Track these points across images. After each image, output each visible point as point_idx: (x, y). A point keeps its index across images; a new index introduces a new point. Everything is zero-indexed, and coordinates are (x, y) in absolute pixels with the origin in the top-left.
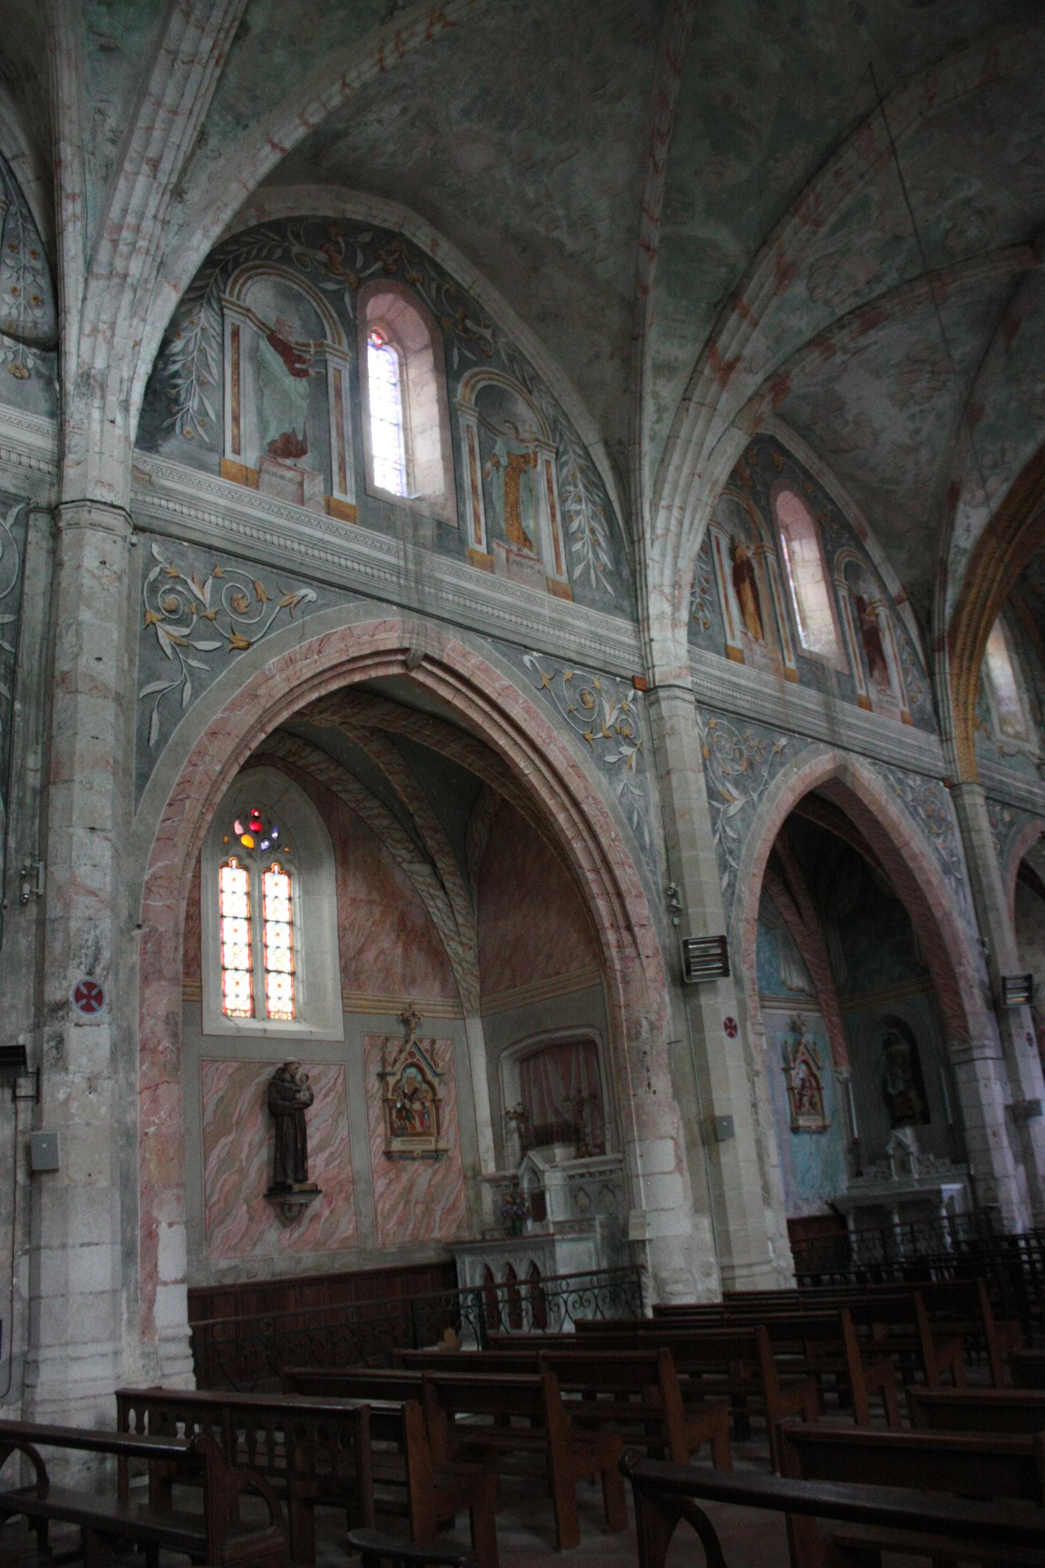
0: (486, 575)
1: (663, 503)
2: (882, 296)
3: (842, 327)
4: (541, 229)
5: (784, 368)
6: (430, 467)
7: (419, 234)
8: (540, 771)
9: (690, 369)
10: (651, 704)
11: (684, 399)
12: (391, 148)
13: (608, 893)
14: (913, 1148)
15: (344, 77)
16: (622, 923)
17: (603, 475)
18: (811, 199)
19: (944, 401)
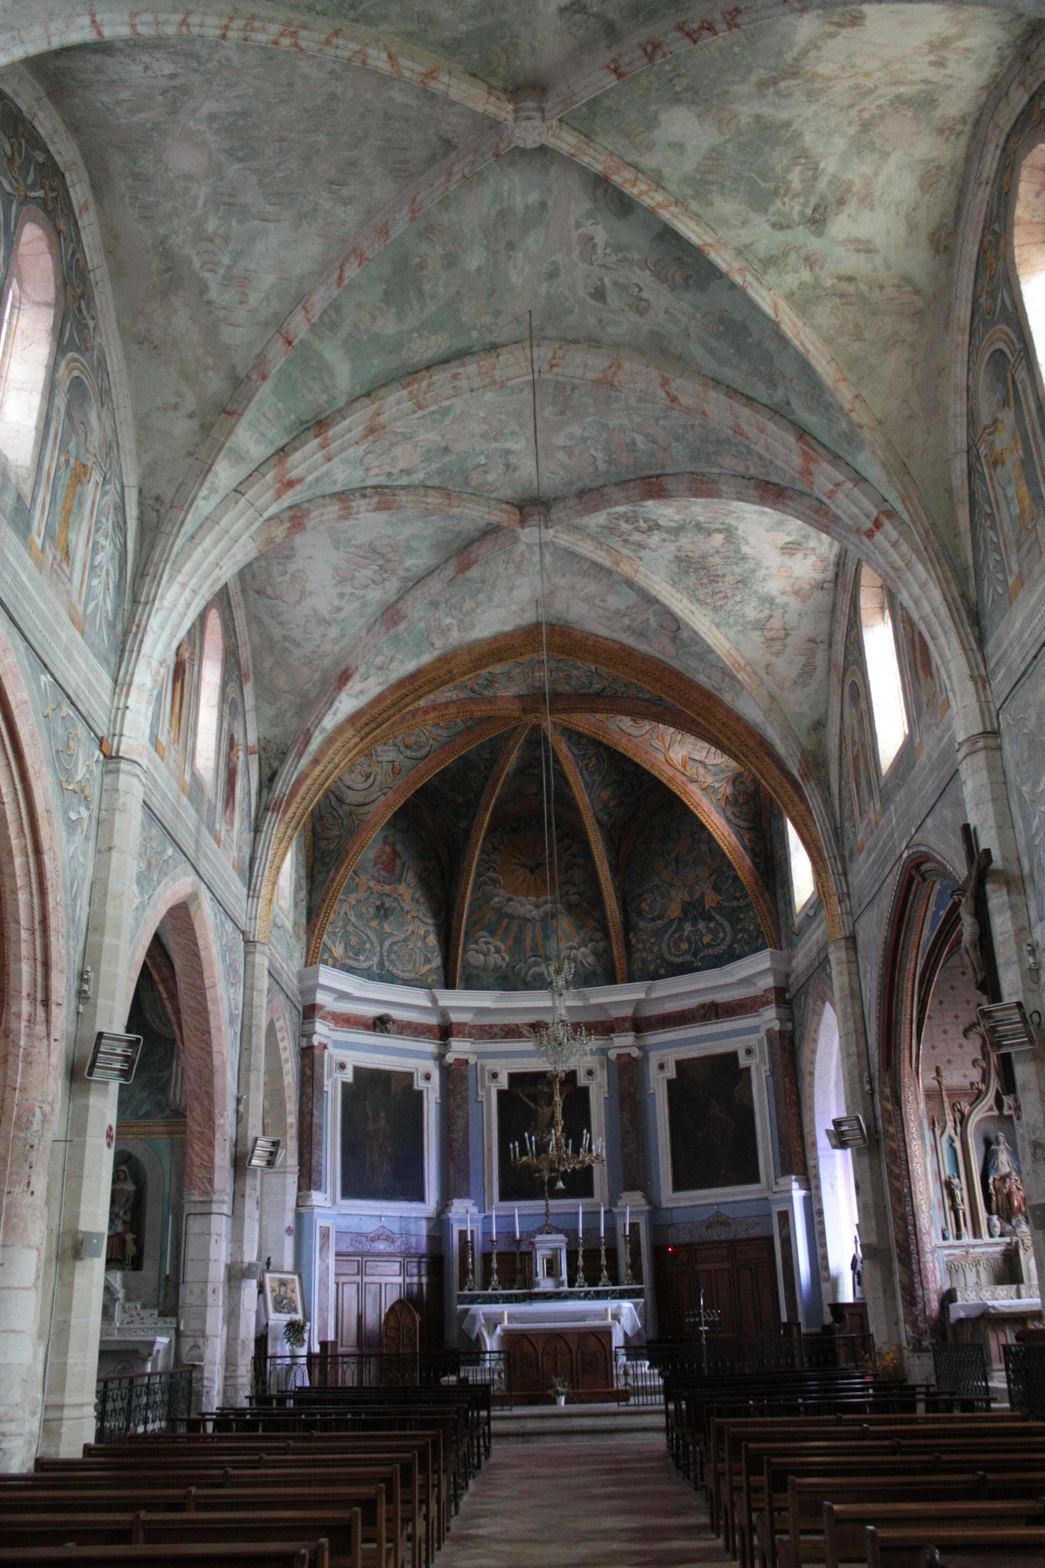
0: (35, 570)
1: (180, 578)
2: (403, 488)
3: (364, 496)
4: (197, 264)
5: (306, 505)
6: (18, 431)
7: (77, 187)
8: (18, 804)
9: (253, 466)
10: (108, 772)
11: (236, 491)
12: (125, 95)
13: (35, 959)
14: (121, 1294)
15: (188, 13)
16: (39, 996)
17: (129, 521)
18: (424, 384)
19: (376, 595)
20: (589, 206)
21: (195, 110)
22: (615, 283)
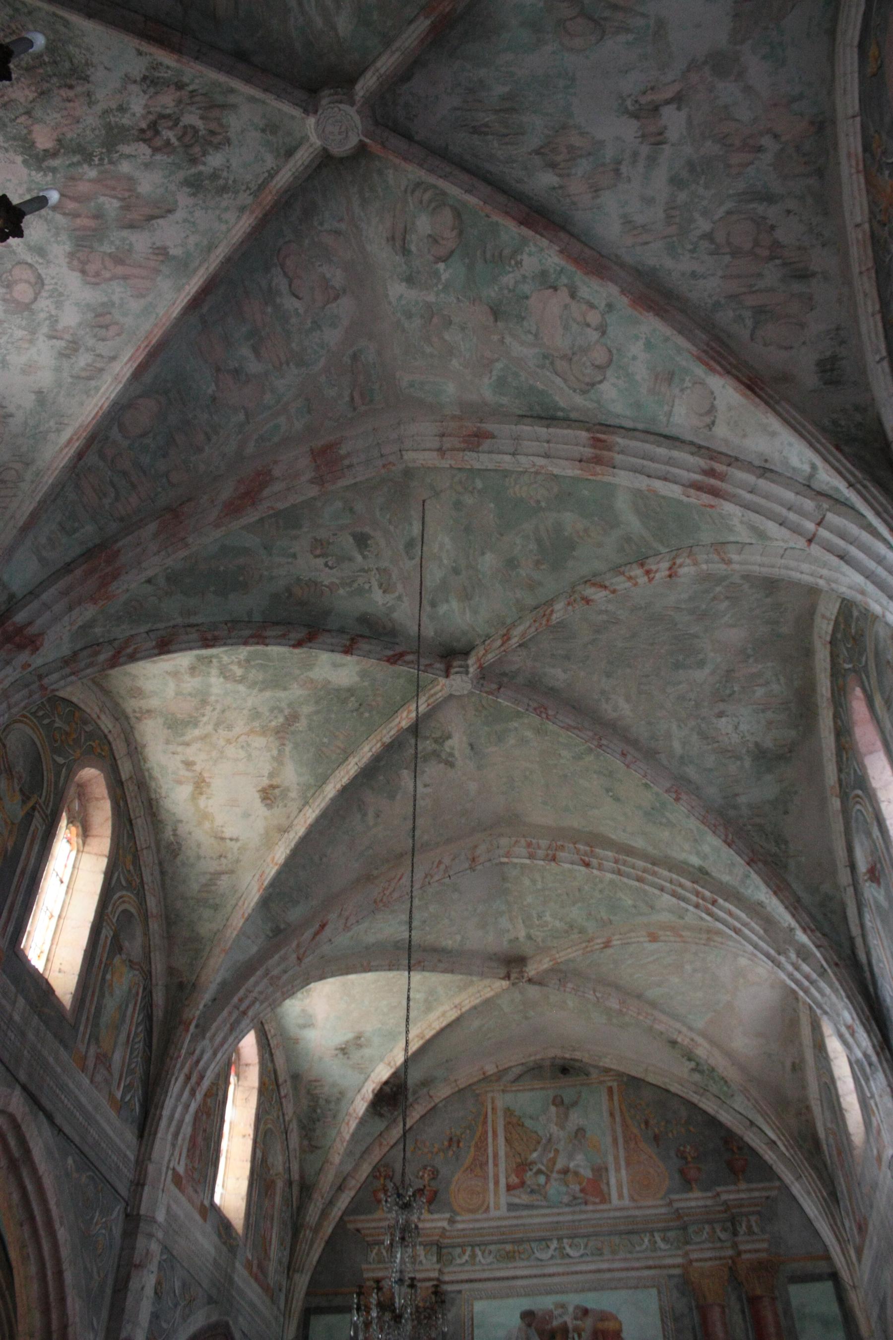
20: (395, 615)
21: (713, 673)
22: (351, 559)
